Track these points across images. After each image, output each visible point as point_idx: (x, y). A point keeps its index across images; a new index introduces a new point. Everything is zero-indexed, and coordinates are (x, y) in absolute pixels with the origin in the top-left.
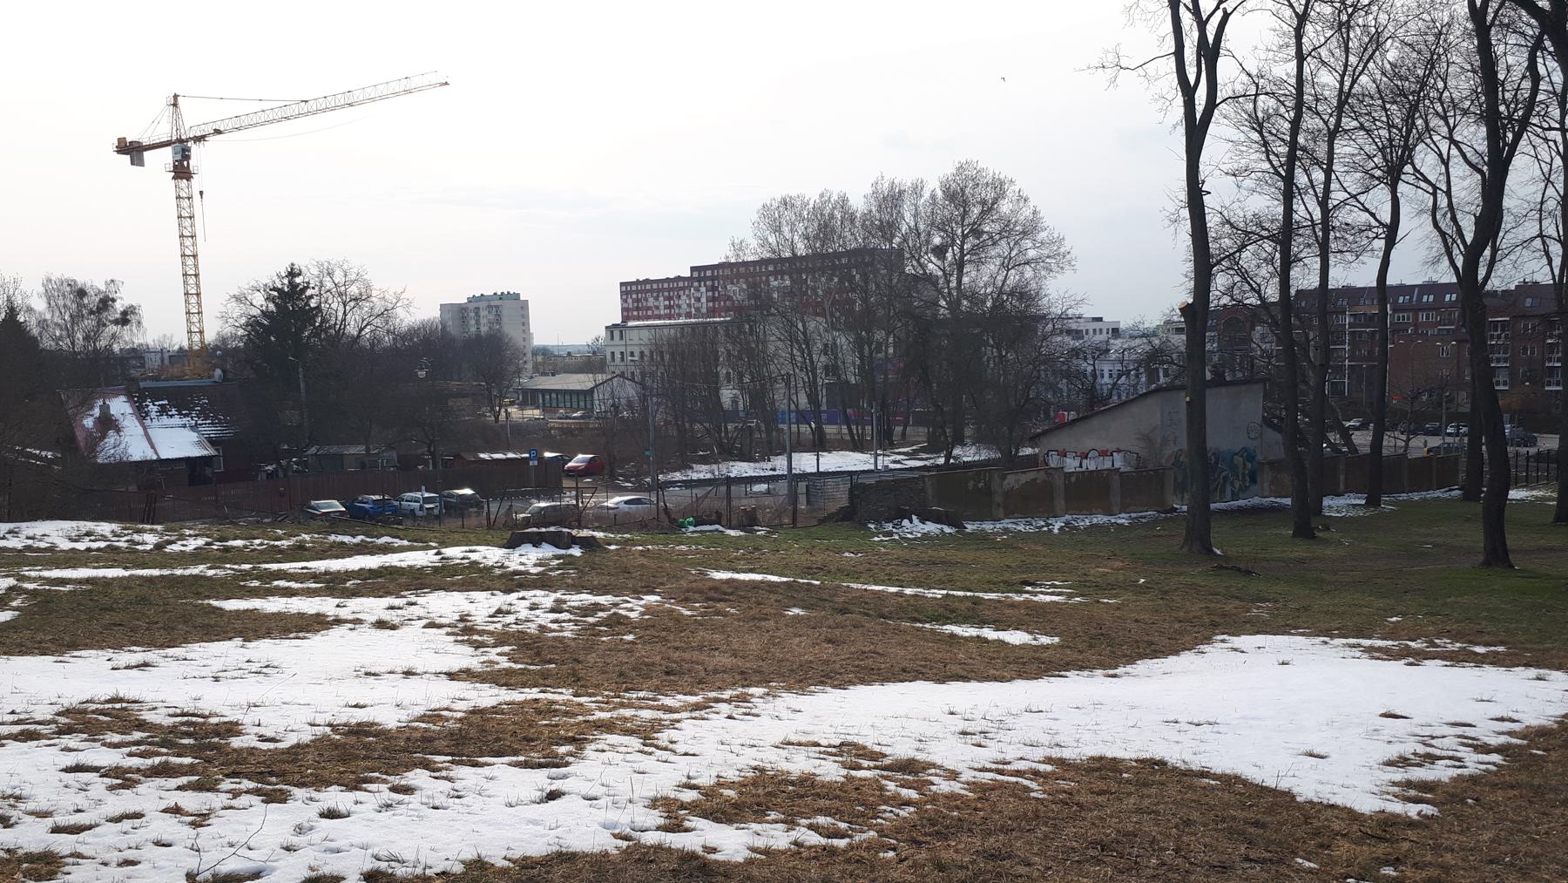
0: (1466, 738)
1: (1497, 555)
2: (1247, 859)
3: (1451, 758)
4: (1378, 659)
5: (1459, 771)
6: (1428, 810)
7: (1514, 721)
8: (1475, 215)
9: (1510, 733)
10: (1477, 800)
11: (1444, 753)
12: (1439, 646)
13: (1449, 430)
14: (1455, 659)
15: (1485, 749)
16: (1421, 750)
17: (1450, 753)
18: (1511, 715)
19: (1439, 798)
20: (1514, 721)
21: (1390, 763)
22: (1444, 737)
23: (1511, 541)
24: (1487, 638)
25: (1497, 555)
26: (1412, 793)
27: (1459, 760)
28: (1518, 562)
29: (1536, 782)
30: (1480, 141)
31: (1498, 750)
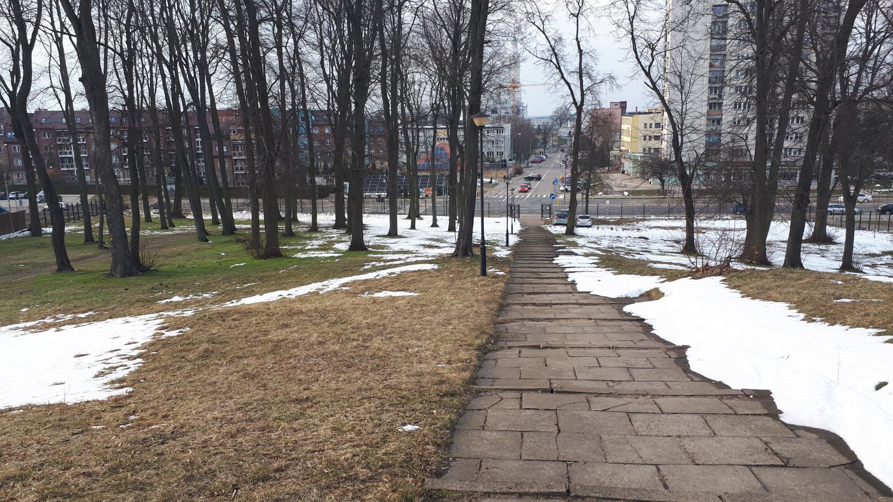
0: (121, 356)
1: (64, 265)
2: (74, 434)
3: (121, 366)
4: (36, 332)
5: (129, 370)
6: (130, 389)
7: (136, 343)
8: (10, 71)
9: (138, 348)
10: (144, 379)
11: (118, 364)
12: (61, 319)
13: (11, 196)
14: (74, 322)
15: (134, 358)
16: (107, 366)
17: (120, 364)
18: (133, 341)
19: (130, 383)
20: (136, 343)
21: (96, 376)
22: (111, 358)
23: (71, 254)
24: (82, 309)
25: (64, 265)
26: (117, 385)
27: (125, 366)
28: (76, 266)
29: (163, 364)
30: (5, 27)
31: (139, 356)
